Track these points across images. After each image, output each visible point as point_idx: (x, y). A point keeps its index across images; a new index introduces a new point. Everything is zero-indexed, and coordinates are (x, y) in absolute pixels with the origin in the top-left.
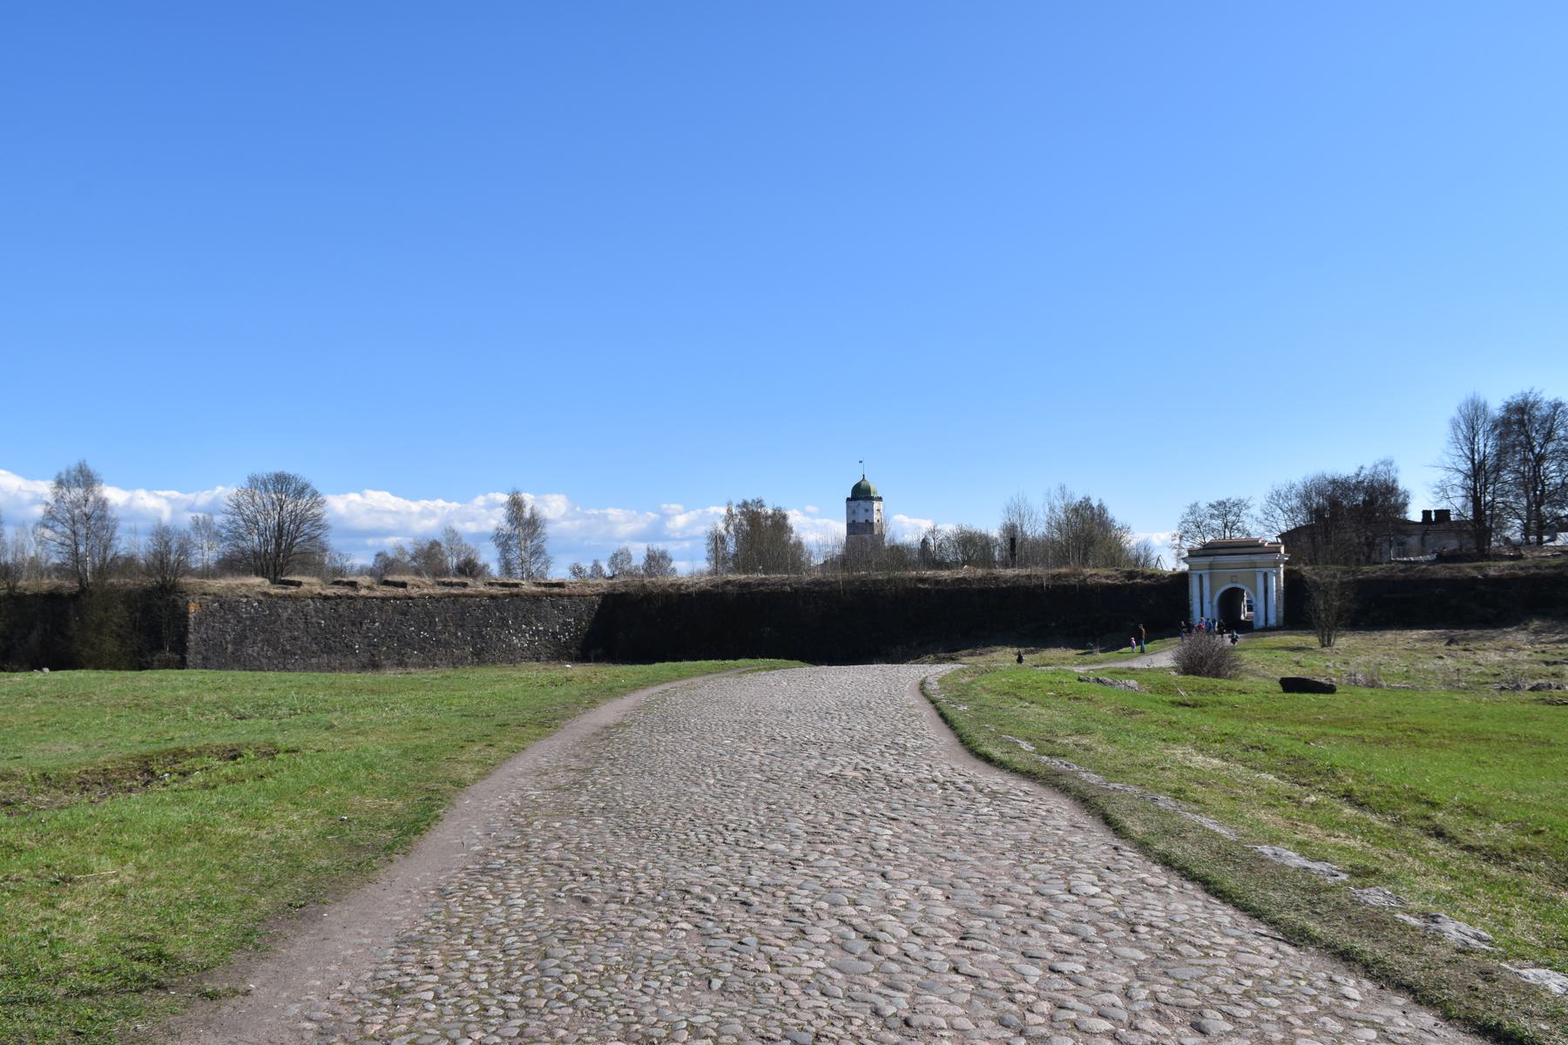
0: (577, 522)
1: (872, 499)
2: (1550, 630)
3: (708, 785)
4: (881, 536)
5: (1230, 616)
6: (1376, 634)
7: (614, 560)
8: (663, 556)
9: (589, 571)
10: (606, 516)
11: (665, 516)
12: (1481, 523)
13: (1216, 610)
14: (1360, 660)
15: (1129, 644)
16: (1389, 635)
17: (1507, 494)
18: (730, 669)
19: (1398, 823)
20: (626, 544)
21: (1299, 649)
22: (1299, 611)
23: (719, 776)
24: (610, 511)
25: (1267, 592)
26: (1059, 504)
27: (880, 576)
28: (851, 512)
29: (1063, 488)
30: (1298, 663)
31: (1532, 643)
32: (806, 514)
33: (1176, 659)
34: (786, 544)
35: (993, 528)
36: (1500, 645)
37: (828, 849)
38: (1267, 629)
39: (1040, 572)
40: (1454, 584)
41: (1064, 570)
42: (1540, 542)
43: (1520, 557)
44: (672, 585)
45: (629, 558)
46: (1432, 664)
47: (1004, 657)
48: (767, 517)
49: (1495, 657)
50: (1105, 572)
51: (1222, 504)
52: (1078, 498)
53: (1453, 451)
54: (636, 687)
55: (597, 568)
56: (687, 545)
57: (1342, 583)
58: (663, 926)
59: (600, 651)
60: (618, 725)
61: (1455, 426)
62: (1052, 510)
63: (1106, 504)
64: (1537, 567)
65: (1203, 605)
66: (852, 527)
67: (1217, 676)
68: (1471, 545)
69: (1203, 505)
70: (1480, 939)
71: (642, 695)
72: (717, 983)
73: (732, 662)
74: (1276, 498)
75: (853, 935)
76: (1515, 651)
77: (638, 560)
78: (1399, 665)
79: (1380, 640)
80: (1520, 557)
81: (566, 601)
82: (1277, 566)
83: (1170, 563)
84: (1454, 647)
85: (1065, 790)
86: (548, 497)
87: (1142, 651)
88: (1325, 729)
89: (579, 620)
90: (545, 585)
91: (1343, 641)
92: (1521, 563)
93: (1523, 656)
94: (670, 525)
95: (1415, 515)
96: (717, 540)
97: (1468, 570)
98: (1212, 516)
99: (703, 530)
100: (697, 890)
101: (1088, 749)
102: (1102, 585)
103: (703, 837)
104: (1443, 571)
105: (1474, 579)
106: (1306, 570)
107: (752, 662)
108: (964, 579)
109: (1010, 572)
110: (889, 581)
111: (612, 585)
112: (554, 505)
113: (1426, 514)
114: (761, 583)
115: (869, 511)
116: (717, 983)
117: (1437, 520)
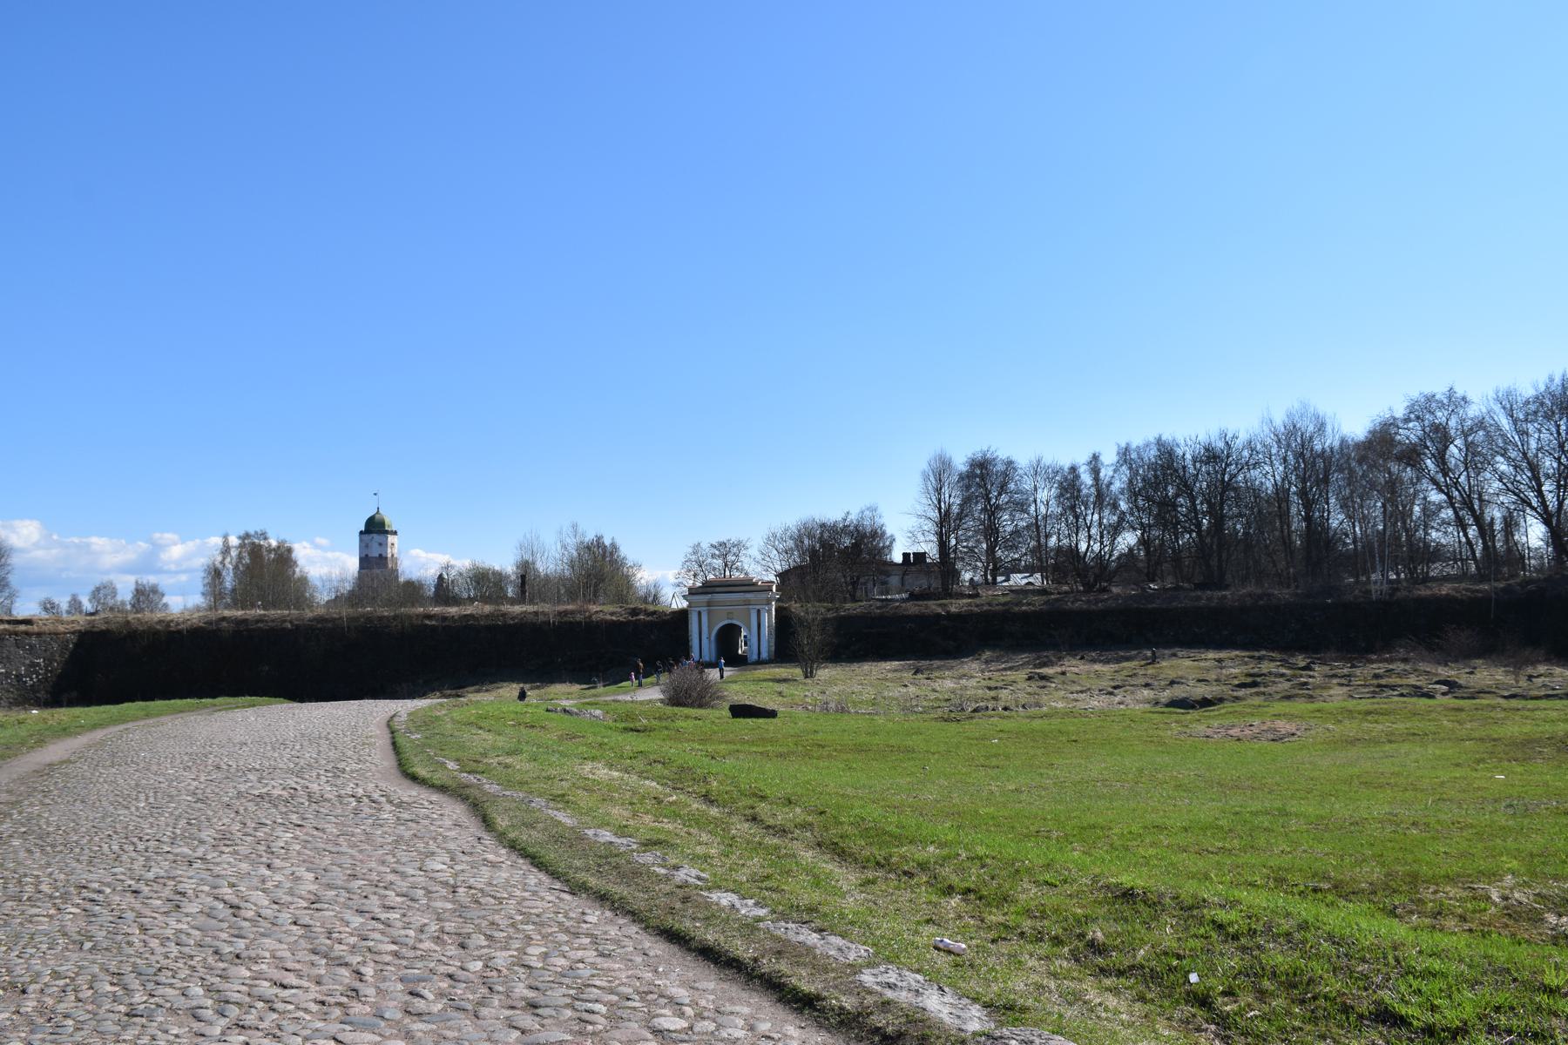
0: (54, 551)
1: (387, 532)
2: (998, 659)
3: (137, 809)
4: (394, 572)
5: (727, 648)
6: (855, 666)
7: (96, 594)
8: (154, 590)
9: (64, 606)
10: (88, 545)
11: (158, 547)
12: (946, 565)
13: (713, 646)
14: (836, 689)
15: (628, 679)
16: (866, 667)
17: (967, 539)
18: (205, 707)
19: (730, 814)
20: (112, 577)
21: (785, 680)
22: (788, 646)
23: (151, 800)
24: (94, 539)
25: (758, 632)
26: (572, 542)
27: (386, 612)
28: (364, 546)
29: (575, 527)
30: (780, 693)
31: (983, 671)
32: (317, 546)
33: (663, 692)
34: (289, 578)
35: (504, 562)
36: (956, 673)
37: (227, 850)
38: (760, 662)
39: (547, 609)
40: (921, 619)
41: (570, 607)
42: (994, 582)
43: (977, 595)
44: (160, 622)
45: (114, 593)
46: (896, 691)
47: (510, 690)
48: (270, 550)
49: (949, 684)
50: (611, 608)
51: (723, 544)
52: (590, 537)
53: (924, 501)
54: (94, 727)
55: (75, 604)
56: (183, 578)
57: (824, 620)
58: (52, 912)
59: (74, 694)
60: (62, 762)
61: (926, 478)
62: (564, 547)
63: (618, 542)
64: (989, 604)
65: (702, 640)
66: (365, 561)
67: (701, 706)
68: (936, 584)
69: (705, 545)
70: (699, 878)
71: (99, 734)
72: (88, 945)
73: (209, 701)
74: (772, 539)
75: (221, 906)
76: (966, 679)
77: (125, 594)
78: (868, 693)
79: (858, 671)
80: (977, 595)
81: (34, 640)
82: (769, 604)
83: (674, 600)
84: (919, 676)
85: (464, 799)
86: (17, 523)
87: (640, 685)
88: (738, 747)
89: (48, 661)
90: (9, 622)
91: (825, 673)
92: (977, 601)
93: (973, 682)
94: (164, 556)
95: (897, 558)
96: (216, 574)
97: (934, 607)
98: (713, 556)
99: (201, 562)
100: (96, 885)
101: (507, 766)
102: (607, 622)
103: (115, 847)
104: (913, 608)
105: (939, 615)
106: (795, 607)
107: (231, 700)
108: (471, 616)
109: (517, 609)
110: (395, 617)
111: (90, 622)
112: (25, 532)
113: (906, 556)
114: (260, 620)
115: (383, 545)
116: (88, 945)
117: (915, 561)
